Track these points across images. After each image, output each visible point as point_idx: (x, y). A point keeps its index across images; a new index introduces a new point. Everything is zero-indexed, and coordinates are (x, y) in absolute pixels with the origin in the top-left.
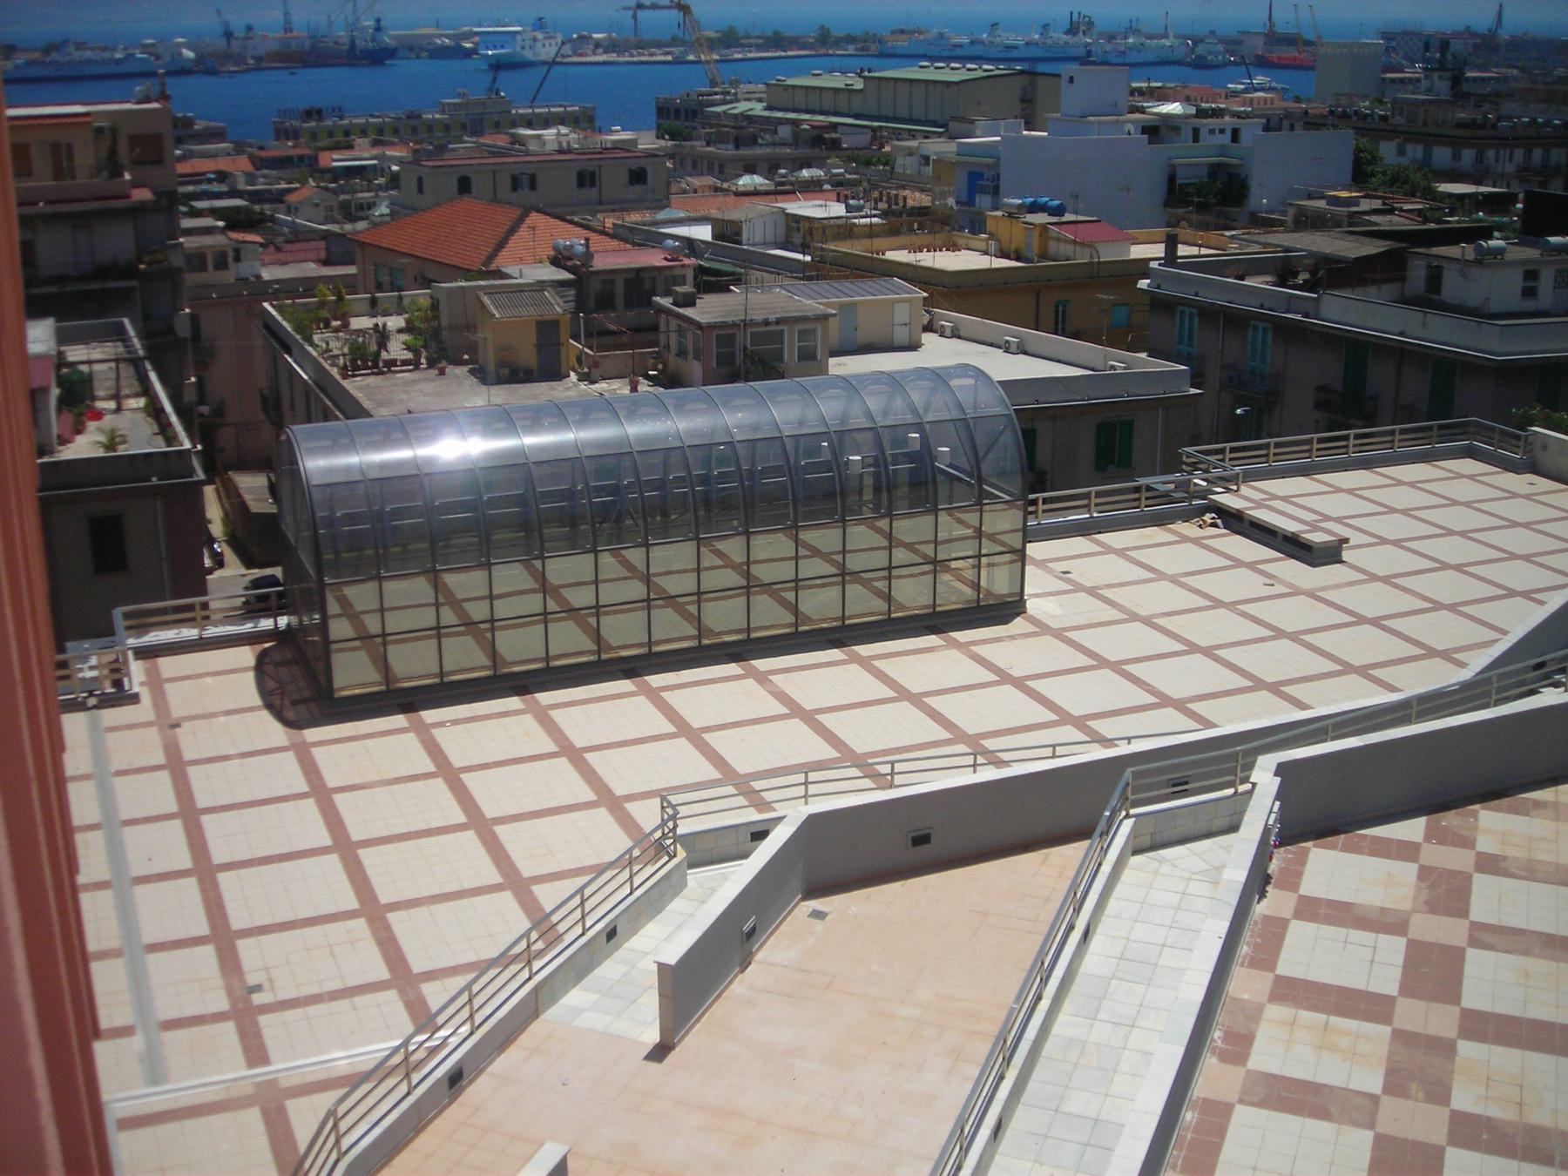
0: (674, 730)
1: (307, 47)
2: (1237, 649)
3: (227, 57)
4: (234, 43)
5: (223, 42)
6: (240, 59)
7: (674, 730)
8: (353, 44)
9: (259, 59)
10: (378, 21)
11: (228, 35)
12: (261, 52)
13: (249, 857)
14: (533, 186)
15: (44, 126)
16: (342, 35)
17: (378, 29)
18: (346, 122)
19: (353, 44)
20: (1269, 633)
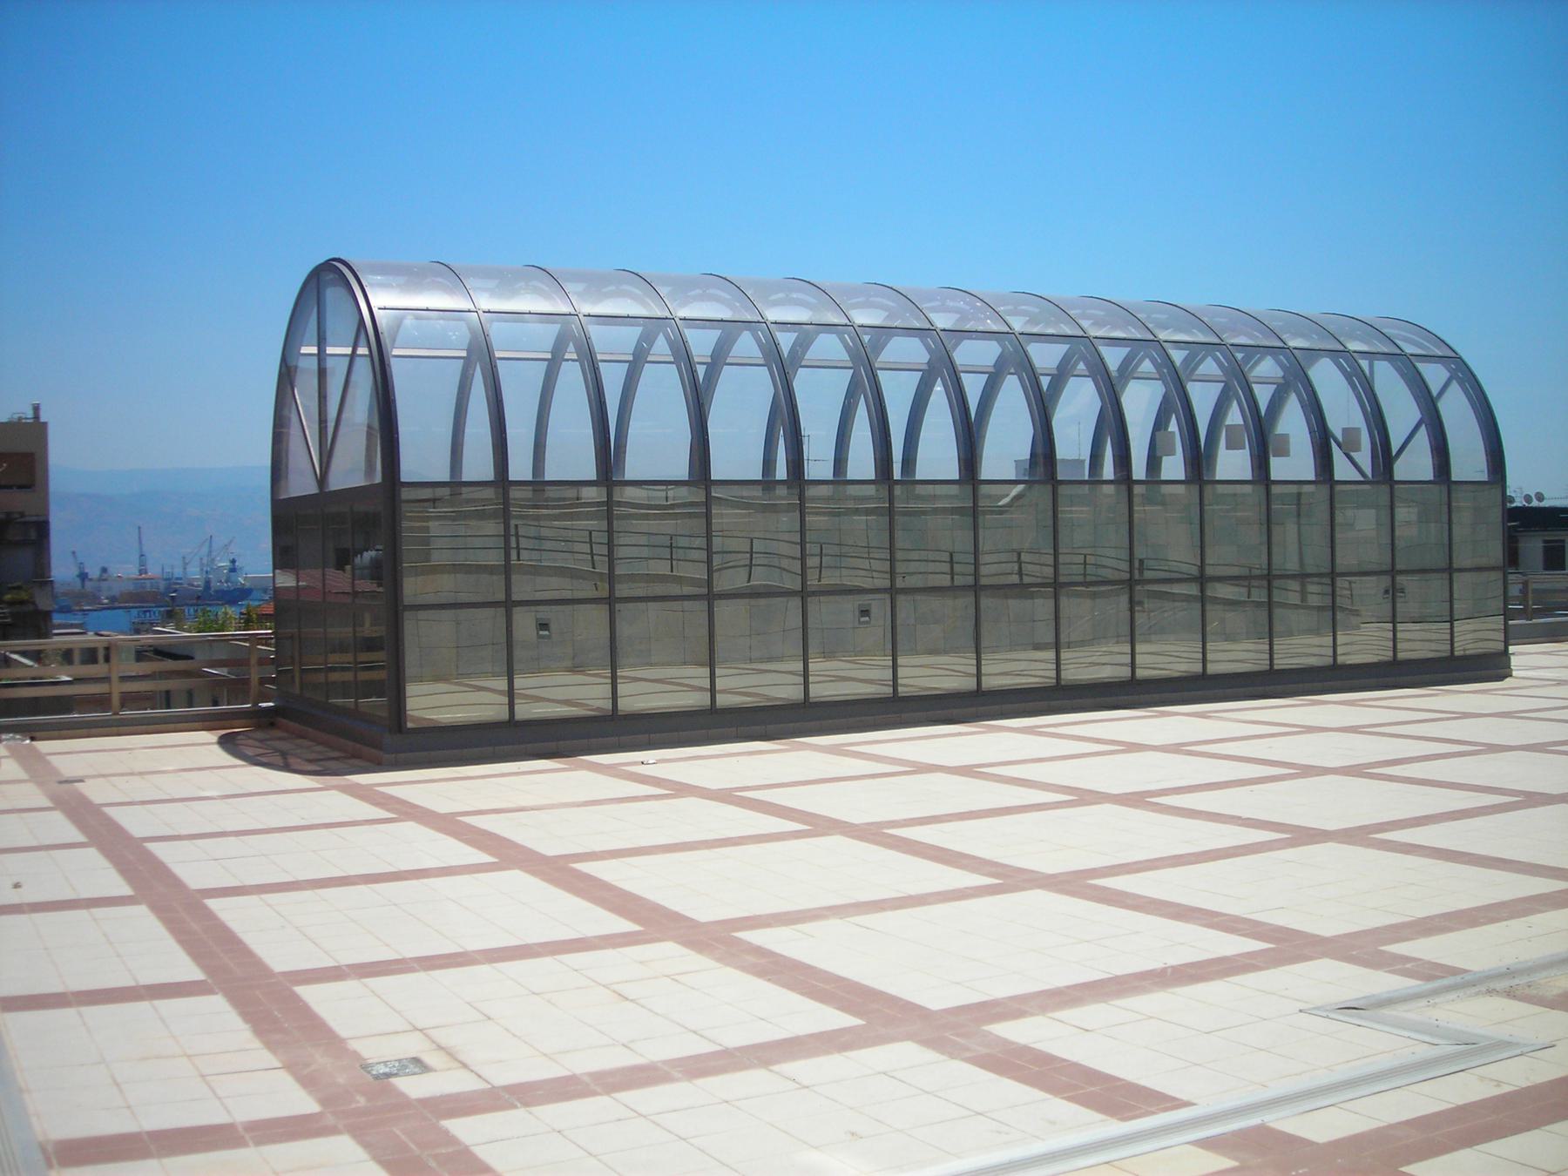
0: (301, 990)
1: (162, 585)
2: (1092, 1013)
3: (81, 596)
4: (88, 584)
5: (78, 581)
6: (94, 598)
7: (301, 990)
8: (208, 583)
9: (113, 599)
10: (233, 561)
11: (83, 576)
12: (115, 592)
13: (57, 988)
14: (107, 659)
15: (1431, 1034)
16: (195, 574)
17: (233, 570)
18: (91, 636)
19: (208, 583)
20: (834, 1019)
